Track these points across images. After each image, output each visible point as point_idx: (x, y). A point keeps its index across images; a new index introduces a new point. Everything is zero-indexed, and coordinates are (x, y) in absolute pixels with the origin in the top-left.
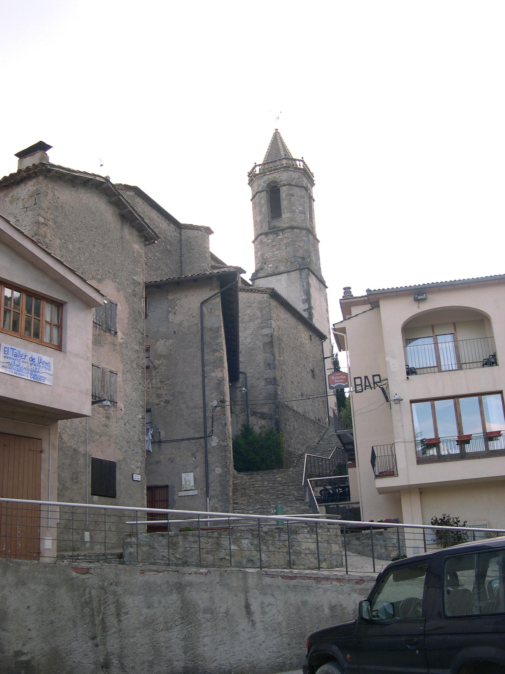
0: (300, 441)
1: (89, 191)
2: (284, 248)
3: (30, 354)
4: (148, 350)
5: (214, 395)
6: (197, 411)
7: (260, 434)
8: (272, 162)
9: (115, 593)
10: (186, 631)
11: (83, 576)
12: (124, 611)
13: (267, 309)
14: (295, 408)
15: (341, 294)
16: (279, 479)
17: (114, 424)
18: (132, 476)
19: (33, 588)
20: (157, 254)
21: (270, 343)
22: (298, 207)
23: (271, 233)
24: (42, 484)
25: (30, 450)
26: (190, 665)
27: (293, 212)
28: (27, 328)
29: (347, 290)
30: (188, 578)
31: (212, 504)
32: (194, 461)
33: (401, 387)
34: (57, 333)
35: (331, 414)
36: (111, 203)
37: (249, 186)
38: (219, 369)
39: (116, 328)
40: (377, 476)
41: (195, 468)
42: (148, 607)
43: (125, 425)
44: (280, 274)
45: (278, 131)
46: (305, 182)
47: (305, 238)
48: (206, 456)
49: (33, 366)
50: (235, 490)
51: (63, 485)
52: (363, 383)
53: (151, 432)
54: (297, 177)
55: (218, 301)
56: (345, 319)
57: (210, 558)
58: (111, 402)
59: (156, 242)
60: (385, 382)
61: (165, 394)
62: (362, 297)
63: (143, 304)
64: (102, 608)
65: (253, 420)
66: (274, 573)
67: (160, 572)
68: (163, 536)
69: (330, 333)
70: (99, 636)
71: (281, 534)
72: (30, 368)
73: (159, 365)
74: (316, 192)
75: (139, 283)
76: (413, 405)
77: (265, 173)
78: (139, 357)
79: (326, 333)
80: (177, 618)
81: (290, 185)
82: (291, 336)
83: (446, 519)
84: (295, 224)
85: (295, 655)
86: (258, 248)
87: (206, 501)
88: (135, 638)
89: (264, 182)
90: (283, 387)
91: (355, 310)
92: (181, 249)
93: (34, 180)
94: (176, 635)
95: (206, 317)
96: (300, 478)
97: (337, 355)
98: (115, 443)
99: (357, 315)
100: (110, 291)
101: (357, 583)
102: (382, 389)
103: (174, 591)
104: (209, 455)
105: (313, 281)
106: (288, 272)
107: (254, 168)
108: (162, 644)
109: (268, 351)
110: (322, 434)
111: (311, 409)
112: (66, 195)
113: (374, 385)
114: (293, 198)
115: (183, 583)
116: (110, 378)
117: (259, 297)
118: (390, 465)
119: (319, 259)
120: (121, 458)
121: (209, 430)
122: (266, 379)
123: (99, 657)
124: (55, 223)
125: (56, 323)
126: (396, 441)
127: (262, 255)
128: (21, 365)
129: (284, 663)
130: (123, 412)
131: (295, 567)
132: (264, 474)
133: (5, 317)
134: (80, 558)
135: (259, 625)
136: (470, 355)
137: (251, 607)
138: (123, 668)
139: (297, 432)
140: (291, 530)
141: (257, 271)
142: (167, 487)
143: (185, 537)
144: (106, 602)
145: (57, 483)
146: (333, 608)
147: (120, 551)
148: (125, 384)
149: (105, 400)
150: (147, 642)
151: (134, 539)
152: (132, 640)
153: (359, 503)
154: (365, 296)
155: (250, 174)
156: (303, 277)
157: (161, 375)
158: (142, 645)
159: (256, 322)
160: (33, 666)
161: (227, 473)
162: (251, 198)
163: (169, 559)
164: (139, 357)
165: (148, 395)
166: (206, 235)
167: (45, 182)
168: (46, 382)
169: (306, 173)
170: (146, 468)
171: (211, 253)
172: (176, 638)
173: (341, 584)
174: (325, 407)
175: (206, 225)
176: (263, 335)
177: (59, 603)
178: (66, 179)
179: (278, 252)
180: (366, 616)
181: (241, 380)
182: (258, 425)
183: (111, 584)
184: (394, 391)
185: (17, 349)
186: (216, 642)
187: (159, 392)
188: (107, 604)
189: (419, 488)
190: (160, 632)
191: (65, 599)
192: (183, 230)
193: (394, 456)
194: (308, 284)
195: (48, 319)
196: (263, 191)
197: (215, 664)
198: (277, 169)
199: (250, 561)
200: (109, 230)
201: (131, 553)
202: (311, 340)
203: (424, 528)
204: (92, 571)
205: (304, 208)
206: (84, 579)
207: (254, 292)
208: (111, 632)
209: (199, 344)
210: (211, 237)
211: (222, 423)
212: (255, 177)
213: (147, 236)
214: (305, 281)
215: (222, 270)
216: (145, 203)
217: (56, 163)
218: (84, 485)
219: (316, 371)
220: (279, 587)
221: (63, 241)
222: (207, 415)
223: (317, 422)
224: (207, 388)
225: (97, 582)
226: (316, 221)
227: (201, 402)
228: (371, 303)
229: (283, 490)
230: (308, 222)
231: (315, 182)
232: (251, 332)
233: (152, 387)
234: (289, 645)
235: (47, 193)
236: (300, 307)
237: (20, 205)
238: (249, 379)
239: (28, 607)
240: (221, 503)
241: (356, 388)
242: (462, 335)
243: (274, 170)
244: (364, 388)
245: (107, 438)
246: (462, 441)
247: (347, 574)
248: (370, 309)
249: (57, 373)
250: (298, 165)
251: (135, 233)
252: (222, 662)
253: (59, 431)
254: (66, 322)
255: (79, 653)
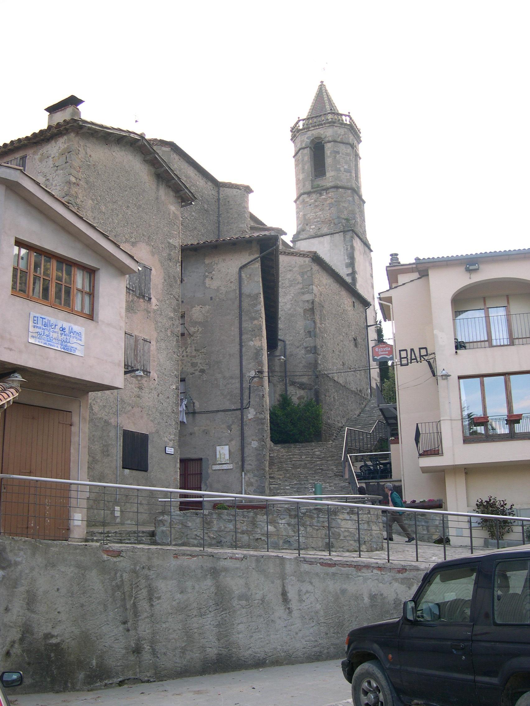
0: (339, 412)
1: (123, 148)
2: (328, 208)
3: (61, 323)
4: (183, 316)
5: (251, 366)
6: (234, 381)
7: (299, 405)
8: (317, 116)
9: (147, 578)
10: (220, 617)
11: (115, 559)
12: (155, 595)
13: (309, 274)
14: (336, 379)
15: (387, 261)
16: (318, 453)
17: (147, 394)
18: (165, 450)
19: (63, 570)
20: (193, 214)
21: (311, 310)
22: (344, 165)
23: (314, 192)
24: (72, 459)
25: (59, 423)
26: (224, 652)
27: (338, 170)
28: (58, 296)
29: (394, 257)
30: (223, 563)
31: (247, 479)
32: (229, 434)
33: (449, 362)
34: (88, 302)
35: (374, 385)
36: (145, 161)
37: (291, 142)
38: (258, 338)
39: (150, 294)
40: (421, 455)
41: (230, 441)
42: (182, 592)
43: (158, 395)
44: (322, 236)
45: (324, 83)
46: (351, 138)
47: (351, 199)
48: (242, 429)
49: (63, 336)
50: (271, 464)
51: (93, 458)
52: (409, 357)
53: (185, 402)
54: (343, 133)
55: (257, 266)
56: (391, 288)
57: (245, 538)
58: (144, 371)
59: (193, 203)
60: (433, 356)
61: (201, 363)
62: (410, 264)
63: (179, 269)
64: (134, 593)
65: (291, 390)
66: (313, 560)
67: (194, 556)
68: (197, 514)
69: (374, 298)
70: (131, 621)
71: (320, 516)
72: (60, 338)
73: (194, 333)
74: (362, 149)
75: (175, 247)
76: (461, 381)
77: (308, 128)
78: (173, 325)
79: (369, 300)
80: (210, 604)
81: (335, 141)
82: (333, 302)
83: (492, 502)
84: (340, 184)
85: (332, 644)
86: (300, 208)
87: (242, 475)
88: (167, 623)
89: (307, 138)
90: (324, 356)
91: (402, 279)
92: (219, 208)
93: (65, 137)
94: (209, 622)
95: (245, 282)
96: (339, 453)
97: (380, 322)
98: (148, 414)
99: (404, 284)
100: (143, 253)
101: (399, 572)
102: (429, 363)
103: (209, 576)
104: (246, 428)
105: (357, 244)
106: (332, 234)
107: (297, 123)
108: (196, 630)
109: (309, 318)
110: (363, 406)
111: (353, 381)
112: (98, 153)
113: (421, 359)
114: (338, 156)
115: (218, 568)
116: (144, 347)
117: (300, 260)
118: (434, 445)
119: (364, 221)
120: (154, 430)
121: (245, 402)
122: (306, 348)
123: (130, 642)
124: (87, 182)
125: (88, 291)
126: (442, 419)
127: (304, 215)
128: (51, 335)
129: (321, 652)
130: (156, 382)
131: (333, 549)
132: (302, 447)
133: (34, 283)
134: (110, 535)
135: (296, 613)
136: (523, 330)
137: (288, 595)
138: (154, 654)
139: (337, 403)
140: (332, 512)
141: (298, 233)
142: (201, 459)
143: (220, 517)
144: (138, 586)
145: (88, 456)
146: (373, 597)
147: (152, 529)
148: (158, 353)
149: (138, 370)
150: (180, 628)
151: (166, 517)
152: (164, 626)
153: (401, 481)
154: (413, 264)
155: (293, 129)
156: (347, 239)
157: (197, 343)
158: (174, 631)
159: (297, 288)
160: (63, 649)
161: (263, 447)
162: (293, 154)
163: (203, 539)
164: (173, 325)
165: (183, 363)
166: (246, 194)
167: (77, 139)
168: (77, 353)
169: (353, 129)
170: (179, 440)
171: (250, 213)
172: (210, 624)
173: (382, 573)
174: (367, 378)
175: (246, 183)
176: (304, 301)
177: (89, 586)
178: (100, 135)
179: (320, 213)
180: (410, 617)
181: (279, 347)
182: (296, 396)
183: (143, 568)
184: (441, 367)
185: (47, 318)
186: (251, 629)
187: (194, 361)
188: (138, 589)
189: (465, 469)
190: (193, 618)
191: (96, 581)
192: (221, 189)
193: (439, 433)
194: (352, 247)
195: (80, 286)
196: (306, 148)
197: (250, 652)
198: (322, 125)
199: (287, 542)
200: (144, 191)
201: (163, 532)
202: (354, 306)
203: (470, 516)
204: (123, 554)
205: (349, 166)
206: (115, 562)
207: (295, 256)
208: (143, 617)
209: (237, 311)
210: (251, 196)
211: (259, 395)
212: (298, 132)
213: (183, 196)
214: (349, 244)
215: (263, 233)
216: (182, 160)
217: (88, 119)
218: (115, 458)
219: (359, 340)
220: (317, 574)
221: (95, 202)
222: (244, 385)
223: (358, 394)
224: (244, 358)
225: (128, 566)
226: (361, 180)
227: (238, 372)
228: (419, 272)
229: (322, 465)
230: (353, 181)
231: (361, 139)
232: (291, 297)
233: (187, 356)
234: (327, 634)
235: (79, 150)
236: (343, 272)
237: (50, 162)
238: (288, 347)
239: (58, 590)
240: (256, 478)
241: (401, 361)
242: (516, 308)
243: (318, 125)
244: (409, 361)
245: (140, 409)
246: (511, 421)
247: (389, 562)
248: (419, 278)
249: (88, 344)
250: (344, 120)
251: (172, 193)
252: (257, 650)
253: (90, 401)
254: (99, 290)
255: (110, 637)
